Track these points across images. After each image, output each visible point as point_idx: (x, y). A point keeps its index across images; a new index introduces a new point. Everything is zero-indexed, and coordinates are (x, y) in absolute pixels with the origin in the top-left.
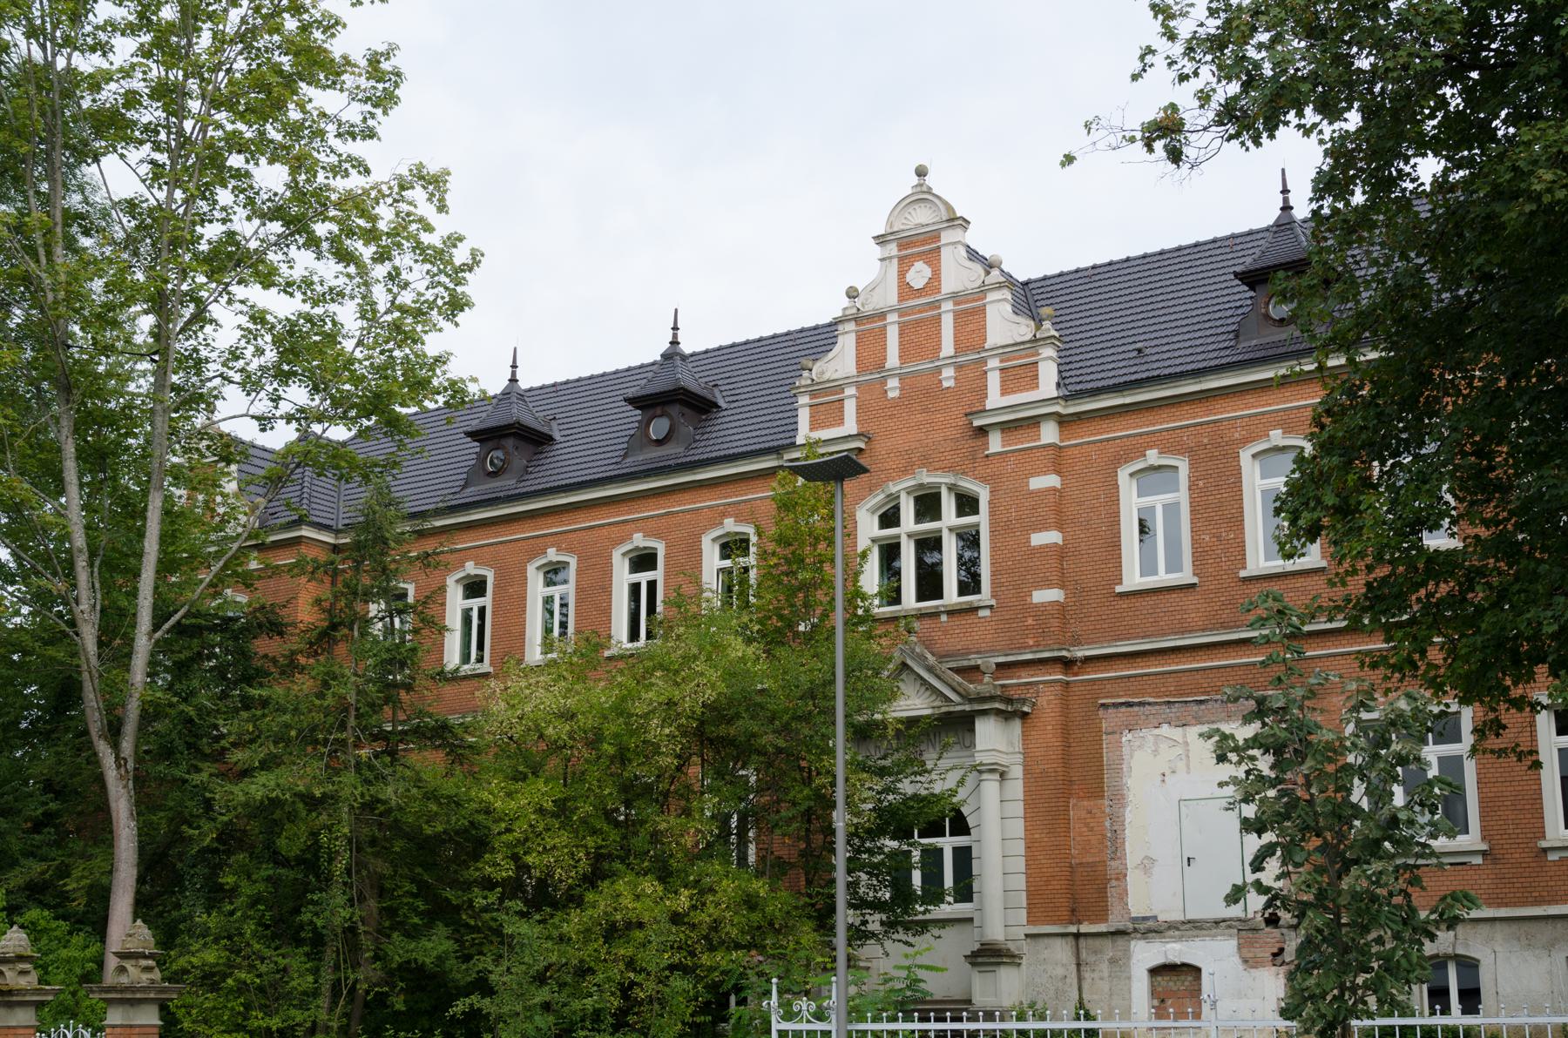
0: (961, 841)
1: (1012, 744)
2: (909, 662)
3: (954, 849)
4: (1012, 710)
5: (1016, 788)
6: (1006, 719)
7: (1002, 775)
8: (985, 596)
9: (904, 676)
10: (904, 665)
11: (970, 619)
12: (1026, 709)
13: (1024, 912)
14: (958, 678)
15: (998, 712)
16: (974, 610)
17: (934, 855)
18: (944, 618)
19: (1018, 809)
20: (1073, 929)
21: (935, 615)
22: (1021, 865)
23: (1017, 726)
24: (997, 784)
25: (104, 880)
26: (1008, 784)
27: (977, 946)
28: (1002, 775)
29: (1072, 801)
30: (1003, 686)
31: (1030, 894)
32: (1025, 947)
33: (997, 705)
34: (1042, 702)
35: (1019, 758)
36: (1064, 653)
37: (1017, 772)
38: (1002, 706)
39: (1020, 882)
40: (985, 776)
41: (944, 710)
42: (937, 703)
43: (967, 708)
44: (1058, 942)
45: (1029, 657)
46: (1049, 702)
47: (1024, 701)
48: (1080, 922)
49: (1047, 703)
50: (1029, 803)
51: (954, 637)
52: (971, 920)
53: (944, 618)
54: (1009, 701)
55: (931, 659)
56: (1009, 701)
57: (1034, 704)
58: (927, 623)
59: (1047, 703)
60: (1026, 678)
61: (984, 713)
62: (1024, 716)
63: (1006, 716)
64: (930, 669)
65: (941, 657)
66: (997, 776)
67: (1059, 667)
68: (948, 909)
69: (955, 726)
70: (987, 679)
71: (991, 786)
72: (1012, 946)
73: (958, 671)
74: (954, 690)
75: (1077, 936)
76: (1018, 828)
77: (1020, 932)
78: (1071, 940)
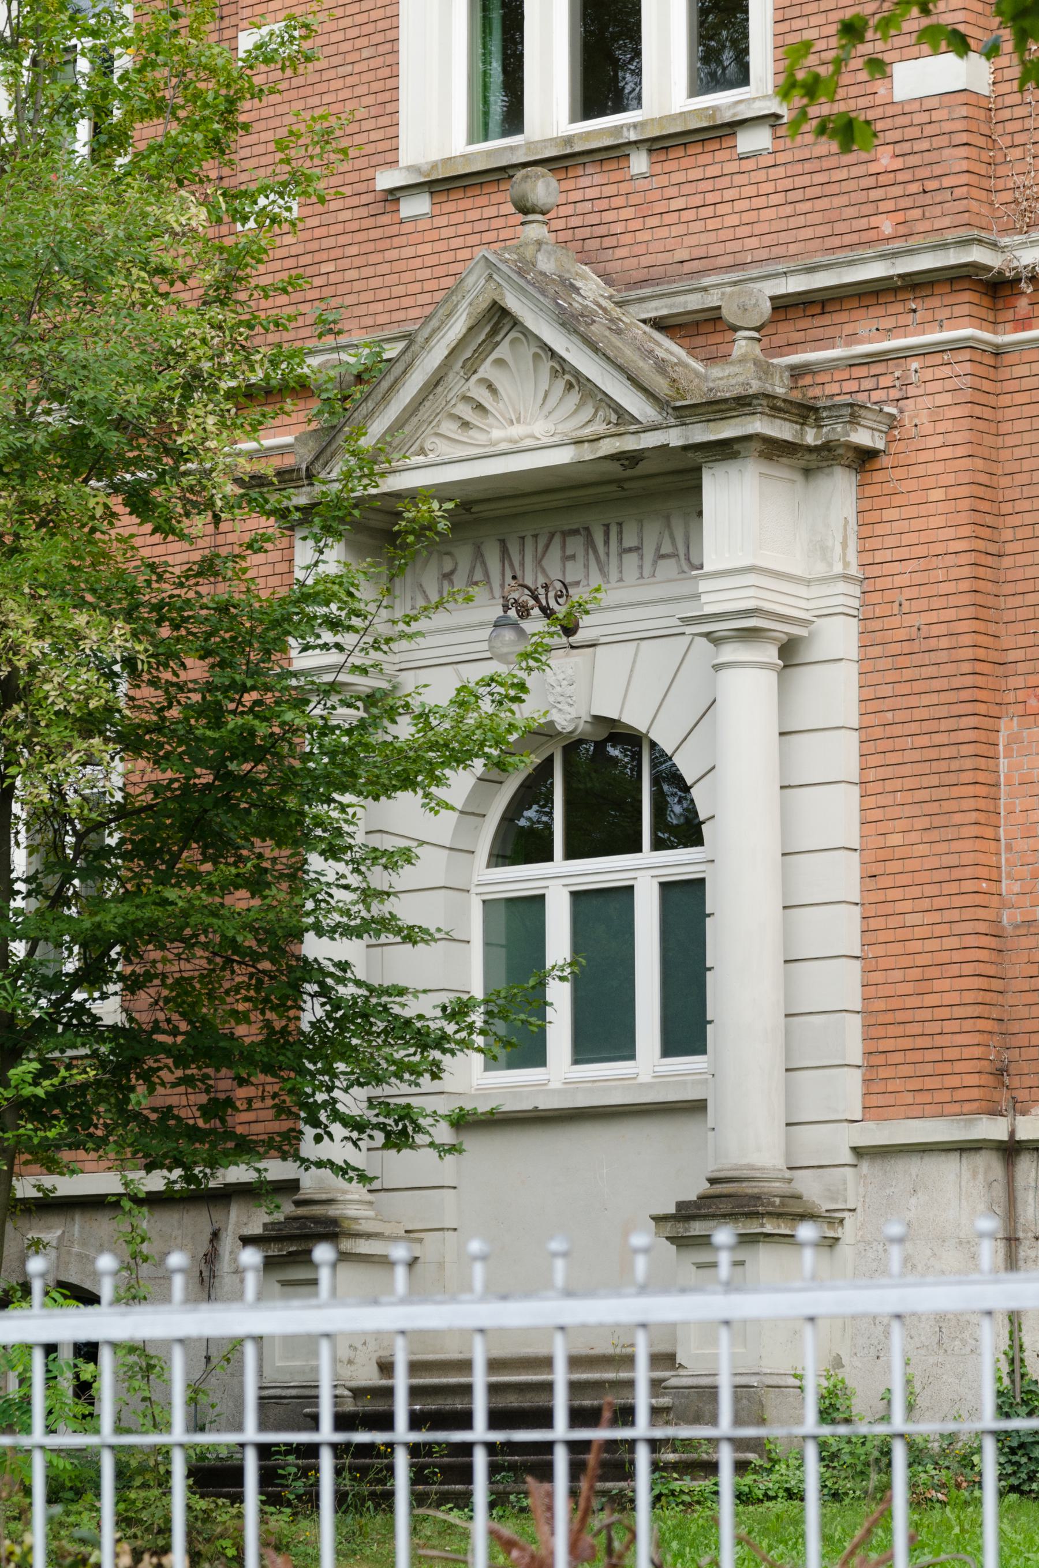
0: (679, 862)
1: (823, 550)
2: (513, 303)
3: (666, 887)
4: (813, 439)
5: (834, 690)
6: (807, 472)
7: (790, 652)
8: (760, 91)
9: (503, 351)
10: (498, 319)
11: (709, 162)
12: (862, 437)
13: (854, 1080)
14: (669, 348)
15: (774, 450)
16: (725, 130)
17: (602, 914)
18: (639, 163)
19: (839, 755)
20: (996, 1129)
21: (613, 154)
22: (843, 931)
23: (840, 490)
24: (769, 679)
25: (741, 1508)
26: (808, 678)
27: (693, 1189)
28: (790, 652)
29: (1007, 728)
30: (797, 372)
31: (878, 1020)
32: (853, 1187)
33: (759, 425)
34: (916, 414)
35: (846, 595)
36: (977, 255)
37: (838, 638)
38: (782, 430)
39: (841, 986)
40: (730, 653)
41: (609, 447)
42: (599, 427)
43: (674, 438)
44: (950, 1167)
45: (876, 270)
46: (936, 414)
47: (854, 413)
48: (1019, 1108)
49: (930, 415)
50: (876, 736)
51: (662, 218)
52: (697, 1107)
53: (639, 163)
54: (806, 412)
55: (591, 288)
56: (806, 412)
57: (893, 423)
58: (591, 181)
59: (930, 415)
60: (869, 337)
61: (725, 450)
62: (864, 459)
63: (811, 461)
64: (571, 322)
65: (628, 287)
66: (770, 654)
67: (966, 300)
68: (648, 1068)
69: (638, 497)
70: (742, 346)
71: (748, 687)
72: (812, 1189)
73: (659, 324)
74: (635, 382)
75: (1010, 1150)
76: (836, 815)
77: (838, 1143)
78: (990, 1164)
